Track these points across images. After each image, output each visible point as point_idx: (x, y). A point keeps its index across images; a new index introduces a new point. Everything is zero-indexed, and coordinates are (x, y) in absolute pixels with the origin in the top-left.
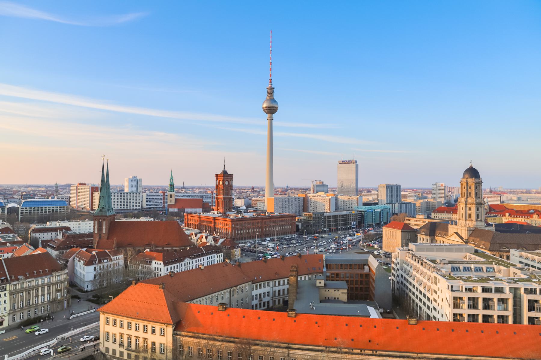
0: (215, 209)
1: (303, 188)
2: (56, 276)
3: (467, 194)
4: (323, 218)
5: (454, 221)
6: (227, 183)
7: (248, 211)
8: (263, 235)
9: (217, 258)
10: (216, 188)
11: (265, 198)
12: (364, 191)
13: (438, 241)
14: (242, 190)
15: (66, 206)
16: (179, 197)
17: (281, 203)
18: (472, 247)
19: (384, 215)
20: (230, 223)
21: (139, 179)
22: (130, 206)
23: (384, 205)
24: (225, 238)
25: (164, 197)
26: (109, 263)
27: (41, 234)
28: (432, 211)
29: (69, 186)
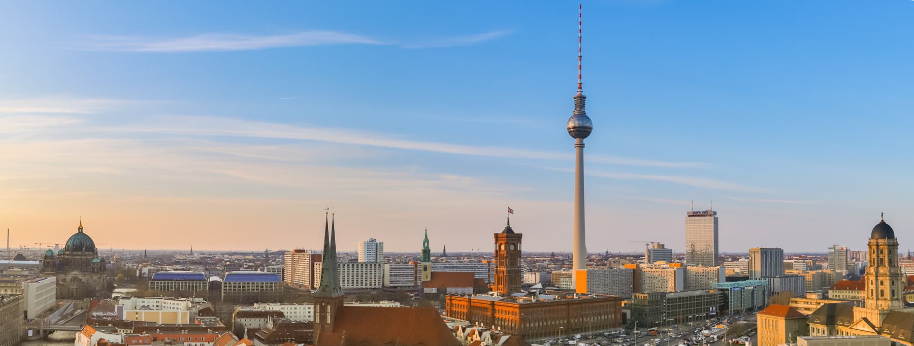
0: (493, 288)
3: (878, 261)
5: (861, 301)
6: (512, 247)
7: (545, 291)
10: (495, 255)
11: (573, 271)
12: (726, 258)
13: (839, 333)
14: (536, 258)
15: (278, 282)
16: (442, 270)
18: (887, 338)
19: (758, 295)
20: (517, 310)
23: (758, 279)
24: (509, 334)
25: (416, 271)
27: (246, 319)
28: (830, 287)
29: (282, 253)
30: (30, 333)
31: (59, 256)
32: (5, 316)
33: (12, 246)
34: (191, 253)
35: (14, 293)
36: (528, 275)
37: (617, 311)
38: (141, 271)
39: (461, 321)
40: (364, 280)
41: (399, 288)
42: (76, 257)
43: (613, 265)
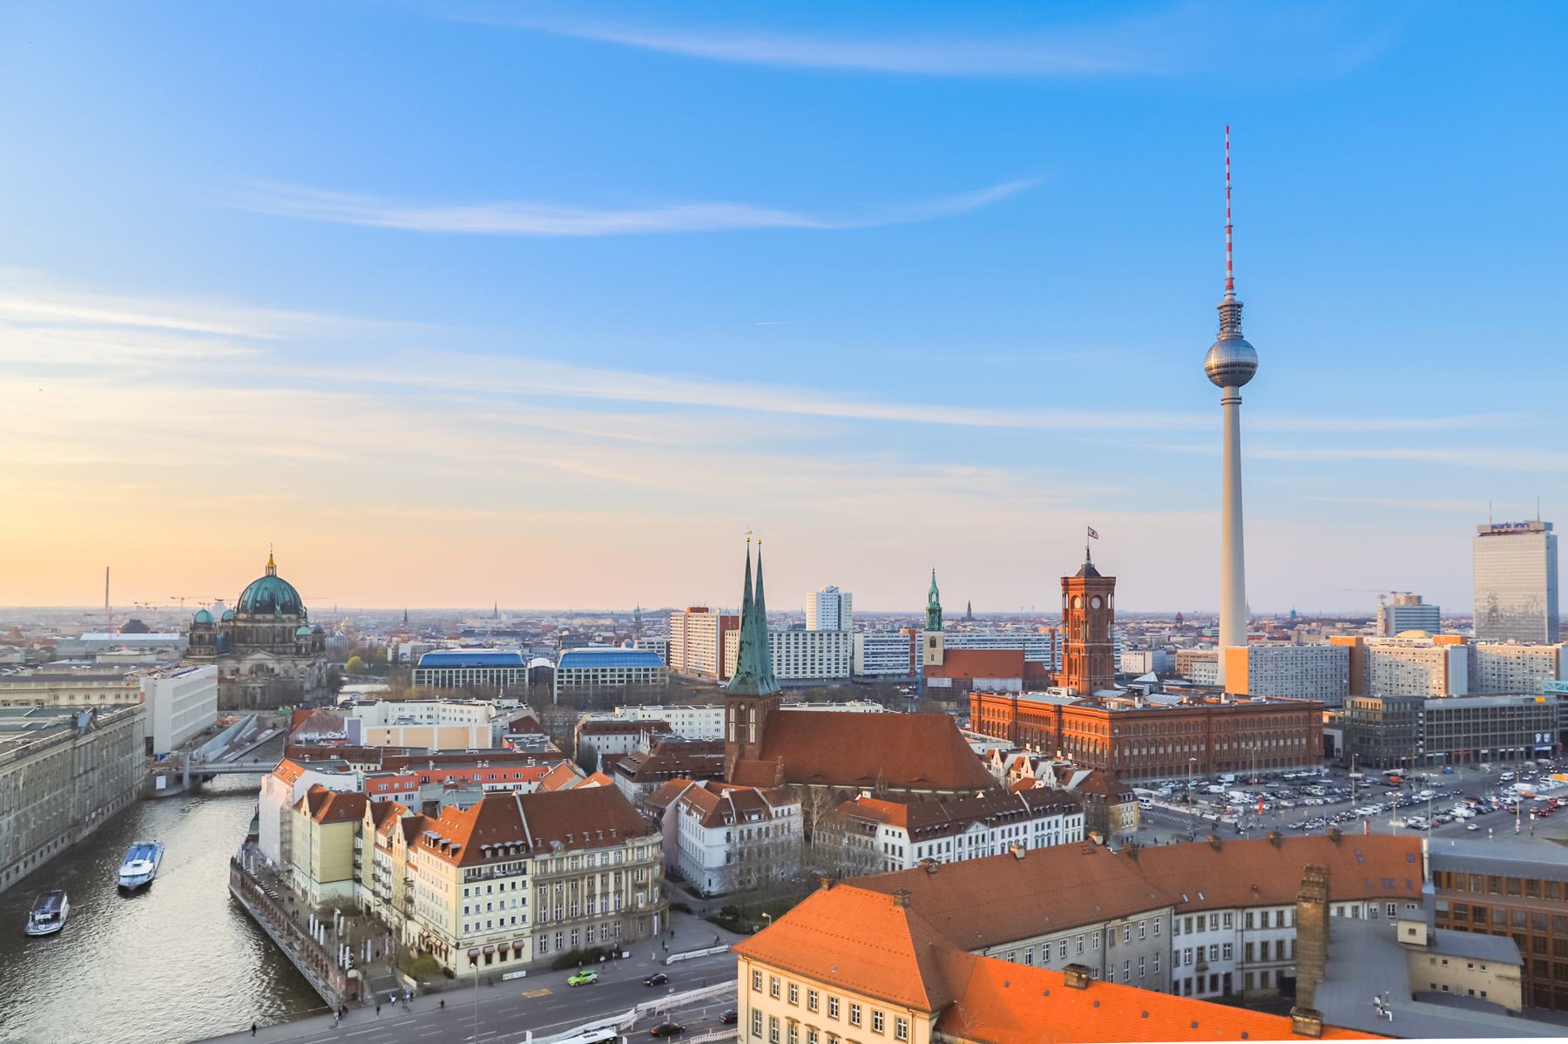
1: (1348, 618)
2: (633, 849)
4: (1421, 715)
6: (1096, 604)
7: (1162, 688)
8: (1211, 764)
9: (1067, 827)
10: (1063, 619)
11: (1220, 650)
17: (1271, 666)
20: (1106, 724)
21: (846, 595)
22: (822, 671)
24: (1091, 768)
25: (913, 646)
26: (763, 825)
27: (601, 737)
29: (667, 614)
30: (161, 783)
31: (225, 624)
32: (102, 749)
33: (116, 603)
34: (496, 615)
35: (122, 701)
36: (1127, 657)
37: (1314, 731)
38: (396, 649)
39: (998, 742)
40: (817, 662)
41: (882, 677)
42: (261, 625)
43: (1305, 637)
